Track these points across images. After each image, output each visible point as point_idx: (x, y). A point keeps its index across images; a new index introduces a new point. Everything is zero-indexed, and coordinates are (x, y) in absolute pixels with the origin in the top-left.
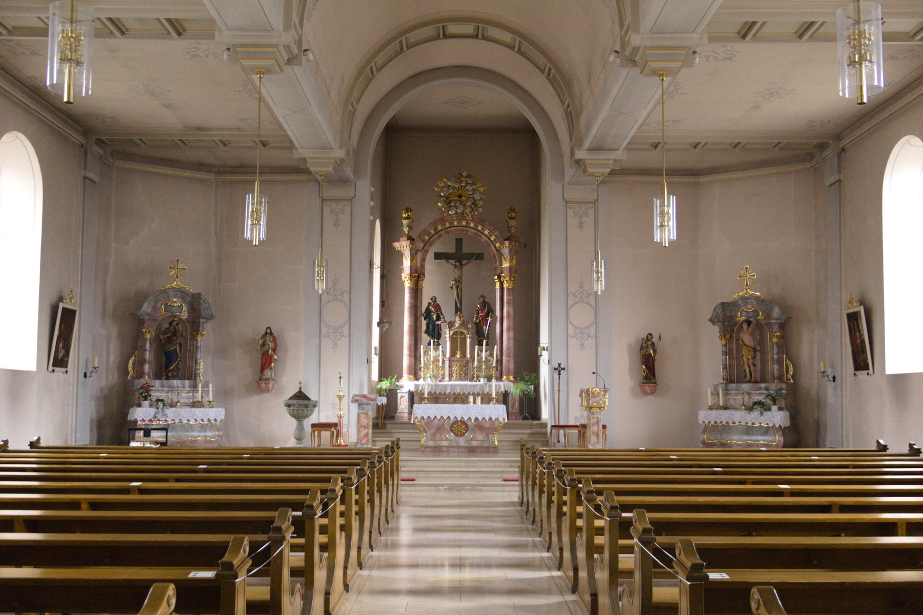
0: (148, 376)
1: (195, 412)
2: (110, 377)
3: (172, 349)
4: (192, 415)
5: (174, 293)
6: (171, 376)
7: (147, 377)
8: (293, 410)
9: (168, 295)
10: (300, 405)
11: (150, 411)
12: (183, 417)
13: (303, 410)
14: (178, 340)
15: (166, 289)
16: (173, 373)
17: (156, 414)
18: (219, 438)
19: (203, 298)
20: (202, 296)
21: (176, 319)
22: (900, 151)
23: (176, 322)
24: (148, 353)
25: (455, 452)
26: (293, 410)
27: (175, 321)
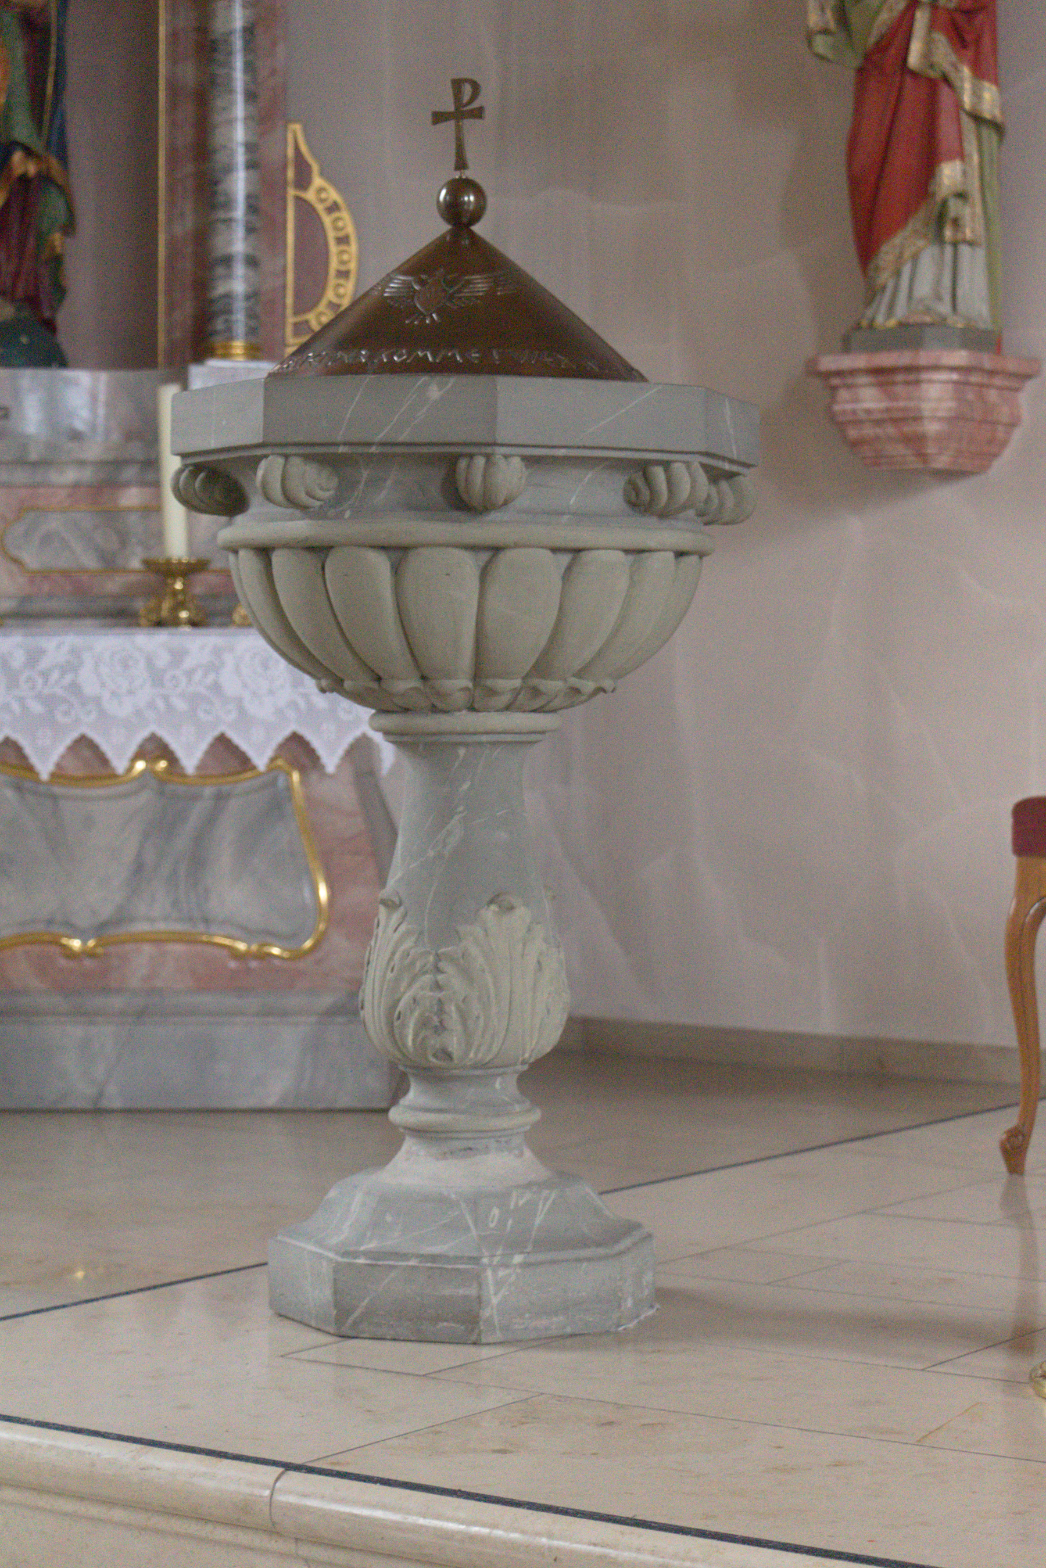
1: (71, 666)
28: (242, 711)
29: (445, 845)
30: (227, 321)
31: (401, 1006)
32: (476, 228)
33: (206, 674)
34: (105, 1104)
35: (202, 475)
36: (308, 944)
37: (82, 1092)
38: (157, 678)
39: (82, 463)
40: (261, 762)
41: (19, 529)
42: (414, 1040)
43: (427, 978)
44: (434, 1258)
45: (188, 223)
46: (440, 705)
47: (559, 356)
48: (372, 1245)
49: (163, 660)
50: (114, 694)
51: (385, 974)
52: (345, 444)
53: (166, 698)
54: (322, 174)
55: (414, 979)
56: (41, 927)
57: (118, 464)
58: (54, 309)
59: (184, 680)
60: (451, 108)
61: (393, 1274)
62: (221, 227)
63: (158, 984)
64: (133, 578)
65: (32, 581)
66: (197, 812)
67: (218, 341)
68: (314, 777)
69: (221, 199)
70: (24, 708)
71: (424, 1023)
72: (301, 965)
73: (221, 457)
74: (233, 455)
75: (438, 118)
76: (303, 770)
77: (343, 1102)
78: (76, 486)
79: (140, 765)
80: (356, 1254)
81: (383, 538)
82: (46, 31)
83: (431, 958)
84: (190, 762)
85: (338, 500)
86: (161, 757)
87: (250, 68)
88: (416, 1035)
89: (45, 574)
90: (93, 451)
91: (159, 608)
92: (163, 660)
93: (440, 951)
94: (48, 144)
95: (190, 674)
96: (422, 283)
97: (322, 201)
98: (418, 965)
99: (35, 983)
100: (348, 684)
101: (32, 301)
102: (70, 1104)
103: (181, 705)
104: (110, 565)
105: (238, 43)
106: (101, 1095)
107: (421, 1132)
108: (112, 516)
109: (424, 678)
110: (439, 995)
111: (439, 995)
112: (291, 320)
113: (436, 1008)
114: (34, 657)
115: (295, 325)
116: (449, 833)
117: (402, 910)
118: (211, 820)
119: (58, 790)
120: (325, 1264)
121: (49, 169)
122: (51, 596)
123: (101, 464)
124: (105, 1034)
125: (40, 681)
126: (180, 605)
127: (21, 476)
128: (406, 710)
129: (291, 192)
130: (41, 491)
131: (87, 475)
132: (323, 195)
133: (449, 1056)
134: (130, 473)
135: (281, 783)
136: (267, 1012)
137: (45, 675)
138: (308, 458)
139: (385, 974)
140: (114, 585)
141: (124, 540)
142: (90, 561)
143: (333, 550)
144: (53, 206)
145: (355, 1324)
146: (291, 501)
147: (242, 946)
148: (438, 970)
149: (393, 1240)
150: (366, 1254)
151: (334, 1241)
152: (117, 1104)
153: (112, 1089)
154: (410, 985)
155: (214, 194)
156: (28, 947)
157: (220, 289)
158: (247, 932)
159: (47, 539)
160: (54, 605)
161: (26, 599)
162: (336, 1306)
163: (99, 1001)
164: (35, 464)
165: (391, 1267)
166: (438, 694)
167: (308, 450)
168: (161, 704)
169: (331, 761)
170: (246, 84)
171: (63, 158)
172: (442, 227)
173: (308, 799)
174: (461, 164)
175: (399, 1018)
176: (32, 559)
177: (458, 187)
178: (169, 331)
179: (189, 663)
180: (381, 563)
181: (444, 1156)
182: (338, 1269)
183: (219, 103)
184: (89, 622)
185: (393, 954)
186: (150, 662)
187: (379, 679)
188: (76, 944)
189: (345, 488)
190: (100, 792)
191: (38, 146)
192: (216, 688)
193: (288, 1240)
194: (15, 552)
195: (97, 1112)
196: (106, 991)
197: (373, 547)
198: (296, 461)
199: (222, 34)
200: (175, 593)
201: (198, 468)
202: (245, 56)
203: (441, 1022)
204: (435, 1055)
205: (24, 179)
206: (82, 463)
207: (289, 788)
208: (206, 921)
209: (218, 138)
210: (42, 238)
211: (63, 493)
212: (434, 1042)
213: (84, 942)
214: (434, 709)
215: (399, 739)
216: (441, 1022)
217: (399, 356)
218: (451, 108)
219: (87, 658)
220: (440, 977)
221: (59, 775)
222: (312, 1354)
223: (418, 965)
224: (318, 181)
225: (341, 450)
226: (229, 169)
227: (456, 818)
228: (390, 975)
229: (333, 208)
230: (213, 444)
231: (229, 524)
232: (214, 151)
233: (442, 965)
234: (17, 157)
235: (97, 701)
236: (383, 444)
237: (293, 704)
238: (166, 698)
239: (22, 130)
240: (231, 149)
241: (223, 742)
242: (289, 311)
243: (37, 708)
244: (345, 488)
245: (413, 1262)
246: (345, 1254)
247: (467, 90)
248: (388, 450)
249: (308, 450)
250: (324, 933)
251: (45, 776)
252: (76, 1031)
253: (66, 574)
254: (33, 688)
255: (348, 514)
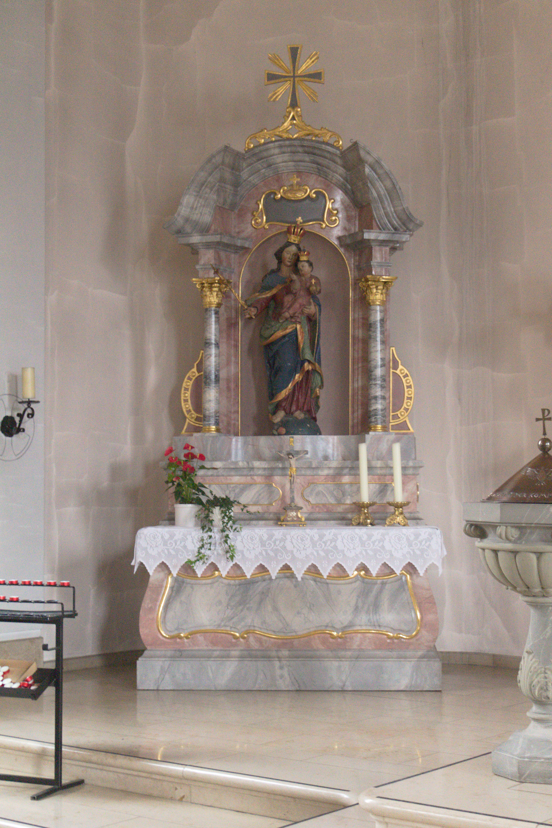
0: (217, 423)
1: (334, 540)
2: (150, 433)
3: (280, 333)
4: (276, 551)
5: (286, 157)
6: (284, 424)
7: (213, 428)
8: (495, 552)
9: (269, 166)
10: (520, 528)
11: (184, 539)
12: (294, 558)
13: (539, 555)
14: (297, 305)
15: (260, 145)
16: (289, 413)
17: (203, 546)
18: (424, 632)
19: (370, 159)
20: (362, 153)
21: (293, 239)
22: (277, 818)
23: (293, 249)
24: (213, 351)
25: (298, 152)
26: (495, 552)
27: (289, 244)
28: (391, 555)
29: (546, 635)
30: (375, 418)
31: (534, 683)
32: (549, 452)
33: (379, 542)
34: (346, 688)
35: (473, 527)
36: (414, 633)
37: (337, 684)
38: (363, 543)
39: (330, 468)
40: (398, 572)
41: (308, 490)
42: (538, 693)
43: (542, 675)
44: (548, 759)
45: (360, 383)
46: (545, 595)
47: (312, 301)
48: (527, 755)
49: (365, 538)
50: (348, 549)
51: (528, 673)
52: (524, 523)
53: (366, 551)
54: (401, 365)
55: (538, 675)
56: (323, 628)
57: (342, 468)
58: (315, 414)
59: (372, 545)
60: (541, 417)
61: (536, 764)
62: (374, 386)
63: (363, 647)
64: (347, 506)
65: (312, 508)
66: (376, 588)
67: (372, 425)
68: (415, 577)
69: (373, 377)
70: (318, 554)
71: (541, 688)
72: (411, 641)
73: (482, 523)
74: (485, 523)
75: (538, 420)
76: (410, 574)
77: (427, 688)
78: (327, 475)
79: (356, 573)
80: (524, 758)
81: (535, 550)
82: (315, 321)
83: (543, 669)
84: (374, 572)
85: (520, 538)
86: (363, 570)
87: (382, 333)
88: (539, 692)
89: (317, 505)
90: (334, 464)
91: (360, 519)
92: (365, 538)
93: (547, 667)
94: (315, 359)
95: (374, 543)
96: (538, 471)
97: (402, 373)
98: (539, 671)
99: (321, 647)
100: (518, 589)
101: (309, 411)
102: (335, 688)
103: (371, 553)
104: (339, 502)
105: (379, 325)
106: (344, 685)
107: (537, 720)
108: (340, 485)
109: (542, 588)
110: (546, 680)
111: (546, 680)
112: (391, 414)
113: (545, 684)
114: (321, 537)
115: (393, 415)
116: (547, 632)
117: (533, 654)
118: (381, 591)
119: (328, 581)
120: (515, 760)
121: (315, 368)
122: (319, 513)
123: (337, 468)
124: (346, 665)
125: (323, 545)
126: (367, 518)
127: (309, 472)
128: (534, 596)
129: (391, 370)
130: (316, 477)
131: (331, 472)
132: (403, 371)
133: (548, 698)
134: (346, 471)
135: (404, 578)
136: (399, 657)
137: (325, 543)
138: (512, 527)
139: (528, 673)
140: (340, 509)
141: (344, 494)
142: (332, 501)
143: (519, 553)
144: (317, 380)
145: (525, 779)
146: (507, 539)
147: (391, 635)
148: (545, 673)
149: (535, 754)
150: (528, 758)
151: (516, 753)
152: (350, 689)
153: (348, 683)
154: (536, 677)
155: (371, 375)
156: (319, 635)
157: (373, 407)
158: (393, 630)
159: (318, 494)
160: (319, 516)
161: (311, 513)
162: (519, 773)
163: (343, 653)
164: (314, 468)
165: (536, 762)
166: (546, 592)
167: (512, 525)
168: (364, 553)
169: (421, 572)
170: (381, 338)
171: (319, 363)
172: (540, 452)
173: (413, 584)
174: (545, 434)
175: (533, 686)
176: (312, 500)
177: (545, 440)
178: (353, 420)
179: (373, 539)
180: (534, 557)
181: (546, 727)
182: (519, 762)
183: (373, 345)
184: (332, 522)
185: (531, 667)
186: (360, 539)
187: (528, 588)
188: (335, 634)
189: (522, 535)
190: (343, 582)
191: (312, 360)
192: (383, 547)
193: (498, 752)
194: (307, 499)
195: (343, 691)
196: (346, 650)
197: (532, 552)
198: (509, 527)
199: (374, 322)
200: (365, 514)
201: (471, 525)
202: (381, 329)
203: (547, 688)
204: (544, 698)
205: (308, 371)
206: (330, 468)
207: (406, 581)
208: (380, 626)
209: (372, 356)
210: (313, 391)
211: (323, 478)
212: (544, 694)
213: (338, 633)
214: (544, 596)
215: (530, 604)
216: (547, 688)
217: (536, 495)
218: (541, 417)
219: (339, 537)
220: (546, 675)
221: (329, 576)
222: (514, 788)
223: (539, 671)
224: (401, 367)
225: (523, 525)
226: (376, 367)
227: (549, 628)
228: (530, 674)
229: (406, 376)
230: (480, 520)
231: (481, 541)
232: (370, 361)
233: (547, 671)
234: (306, 364)
235: (343, 551)
236: (536, 524)
237: (409, 553)
238: (366, 551)
239: (308, 355)
240: (377, 360)
241: (385, 565)
242: (391, 411)
243: (322, 554)
244: (522, 535)
245: (542, 760)
246: (521, 758)
247: (546, 412)
248: (537, 525)
249: (512, 525)
250: (419, 631)
251: (325, 577)
252: (336, 664)
253: (324, 505)
254: (321, 547)
255: (524, 542)
